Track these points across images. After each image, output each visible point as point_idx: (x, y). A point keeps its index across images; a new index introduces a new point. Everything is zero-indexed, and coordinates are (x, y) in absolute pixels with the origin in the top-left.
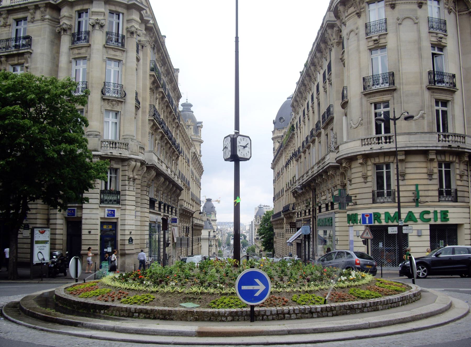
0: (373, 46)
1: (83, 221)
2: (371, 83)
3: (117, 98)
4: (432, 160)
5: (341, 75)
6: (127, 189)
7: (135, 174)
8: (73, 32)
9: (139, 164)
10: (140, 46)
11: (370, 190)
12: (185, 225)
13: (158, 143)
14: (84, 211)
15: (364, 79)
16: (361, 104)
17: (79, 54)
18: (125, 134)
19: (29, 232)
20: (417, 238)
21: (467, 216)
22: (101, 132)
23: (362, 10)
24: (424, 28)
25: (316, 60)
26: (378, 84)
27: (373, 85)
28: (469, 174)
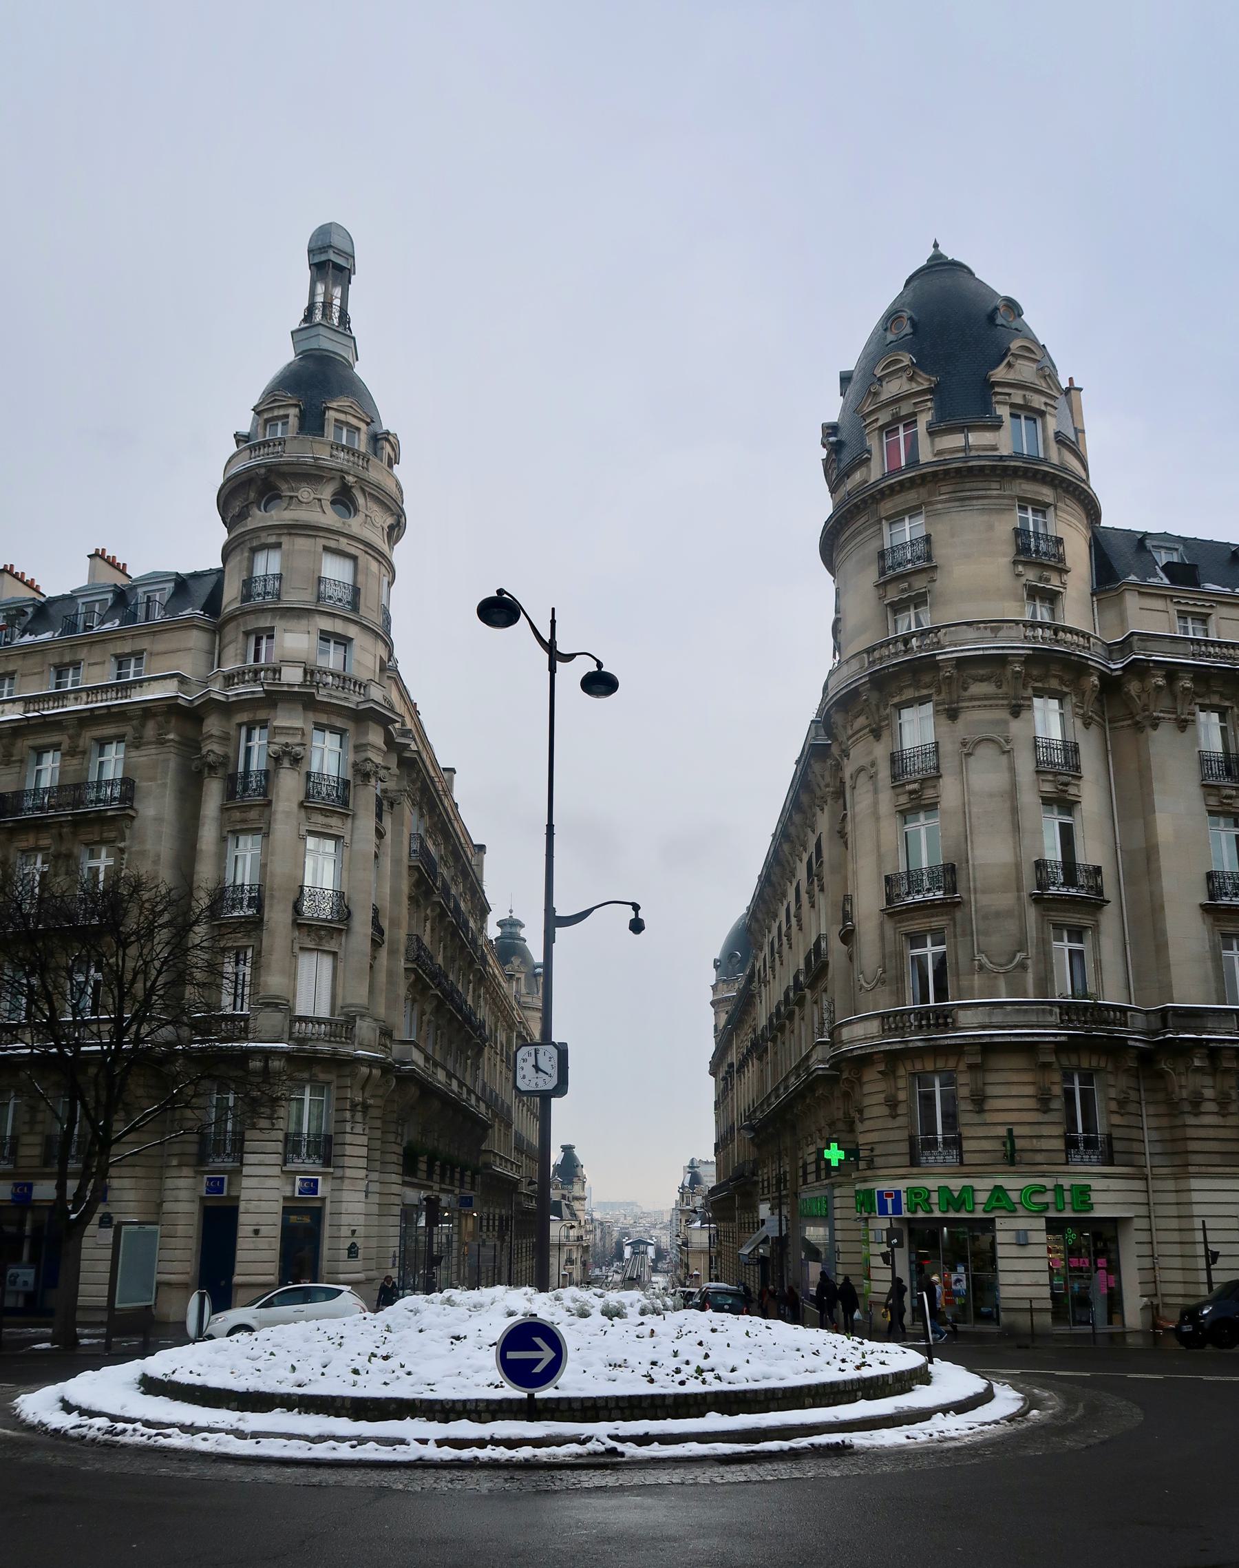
0: (909, 806)
1: (242, 1206)
2: (904, 889)
3: (330, 921)
4: (1046, 1066)
5: (841, 867)
6: (348, 1129)
7: (366, 1095)
8: (230, 771)
9: (376, 1072)
10: (385, 804)
11: (904, 1134)
12: (497, 1211)
13: (429, 1022)
14: (246, 1182)
15: (888, 879)
16: (882, 938)
17: (244, 821)
18: (349, 1001)
19: (110, 1232)
20: (1014, 1251)
21: (1141, 1198)
22: (290, 997)
23: (884, 724)
24: (1025, 765)
25: (792, 830)
26: (918, 892)
27: (908, 894)
28: (1143, 1097)
